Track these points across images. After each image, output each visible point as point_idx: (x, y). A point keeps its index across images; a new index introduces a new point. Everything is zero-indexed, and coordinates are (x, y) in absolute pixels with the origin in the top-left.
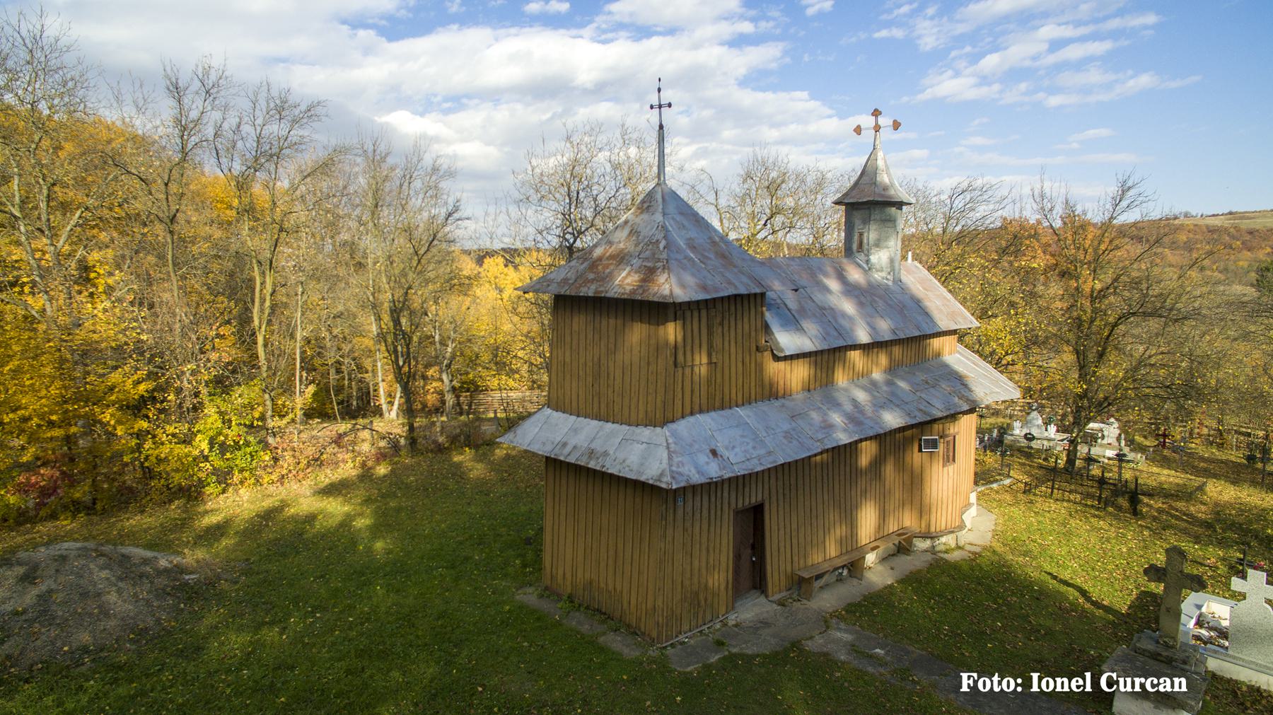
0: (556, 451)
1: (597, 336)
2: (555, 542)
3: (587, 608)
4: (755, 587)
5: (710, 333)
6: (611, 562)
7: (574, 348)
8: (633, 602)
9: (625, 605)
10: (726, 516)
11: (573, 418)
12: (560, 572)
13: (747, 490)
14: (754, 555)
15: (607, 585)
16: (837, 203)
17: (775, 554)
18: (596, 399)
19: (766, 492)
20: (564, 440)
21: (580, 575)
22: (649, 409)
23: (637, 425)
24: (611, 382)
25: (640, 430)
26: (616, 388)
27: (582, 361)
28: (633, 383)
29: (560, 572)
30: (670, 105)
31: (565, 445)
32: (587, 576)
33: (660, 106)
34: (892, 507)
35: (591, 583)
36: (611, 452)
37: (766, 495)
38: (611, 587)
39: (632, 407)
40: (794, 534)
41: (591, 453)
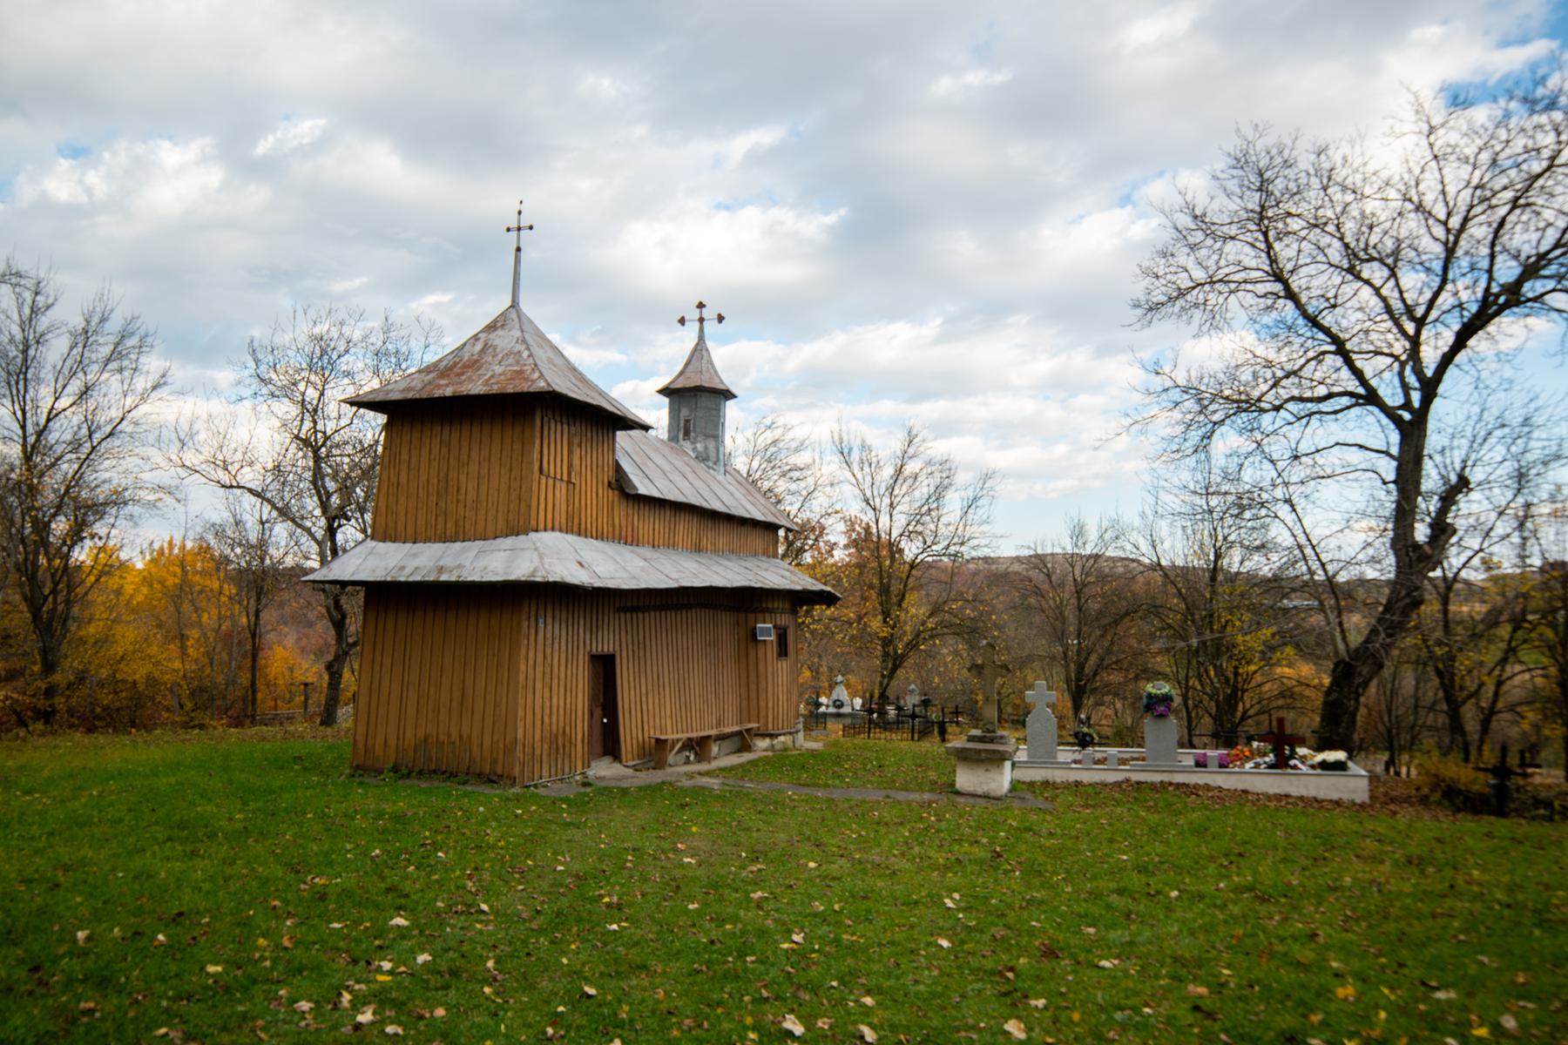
0: (393, 573)
1: (444, 451)
2: (374, 705)
3: (421, 772)
4: (605, 753)
5: (570, 452)
6: (455, 705)
7: (412, 466)
8: (487, 743)
9: (475, 750)
10: (581, 657)
11: (408, 545)
12: (380, 740)
13: (600, 633)
14: (604, 716)
15: (449, 735)
16: (665, 391)
17: (627, 716)
18: (440, 520)
19: (617, 643)
20: (401, 564)
21: (409, 735)
22: (511, 518)
23: (495, 538)
24: (462, 497)
25: (499, 541)
26: (469, 502)
27: (424, 478)
28: (491, 492)
29: (380, 740)
30: (531, 228)
31: (403, 568)
32: (421, 733)
33: (519, 229)
34: (731, 782)
35: (426, 740)
36: (467, 564)
37: (617, 648)
38: (455, 737)
39: (489, 518)
40: (644, 699)
41: (441, 570)
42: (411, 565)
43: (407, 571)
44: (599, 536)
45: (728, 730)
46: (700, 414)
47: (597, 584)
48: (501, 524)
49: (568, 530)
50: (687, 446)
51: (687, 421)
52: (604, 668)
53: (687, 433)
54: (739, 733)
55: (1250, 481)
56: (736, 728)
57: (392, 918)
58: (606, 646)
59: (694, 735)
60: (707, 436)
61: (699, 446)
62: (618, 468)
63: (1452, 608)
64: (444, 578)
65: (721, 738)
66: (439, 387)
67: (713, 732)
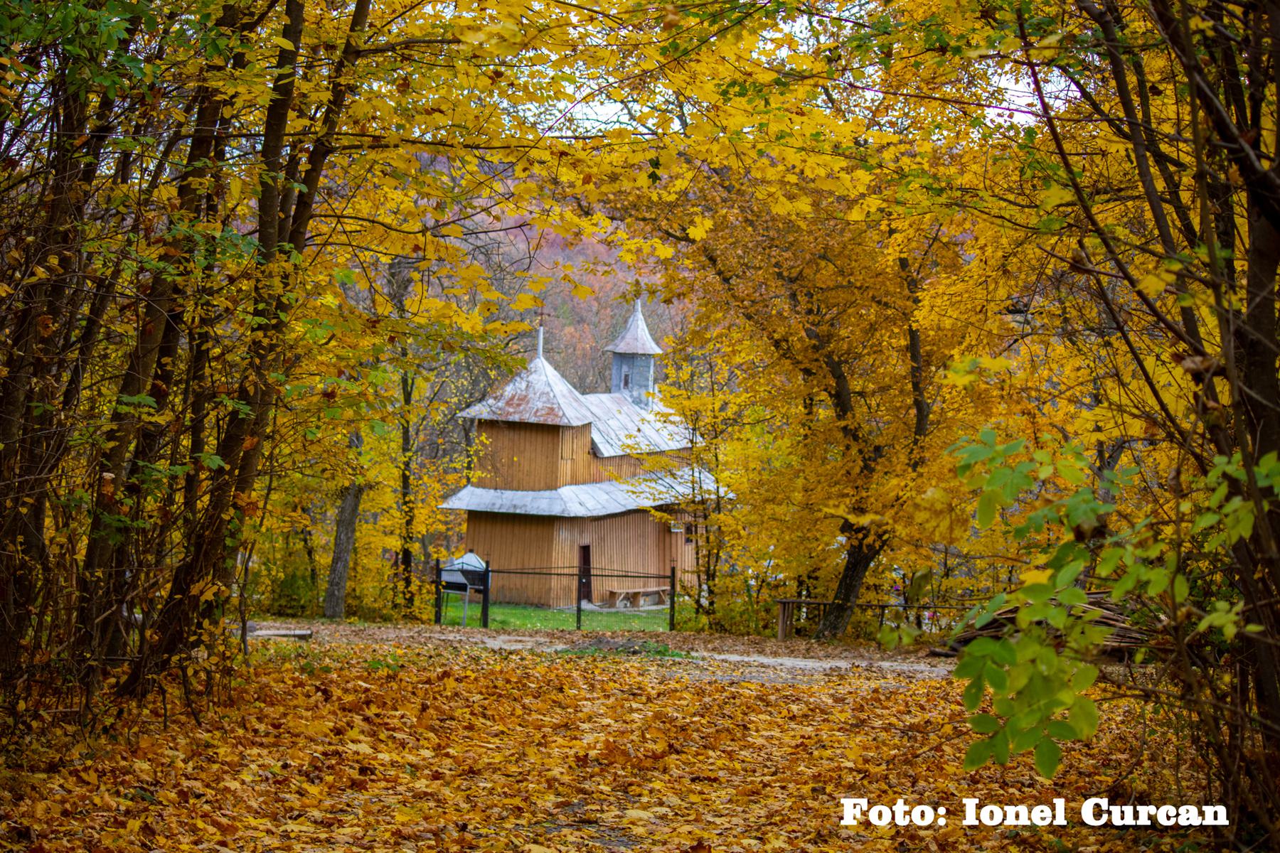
41: (515, 506)
42: (498, 503)
43: (497, 506)
44: (584, 483)
45: (650, 590)
46: (636, 371)
47: (589, 514)
48: (542, 485)
49: (571, 484)
50: (626, 393)
51: (626, 376)
52: (585, 551)
53: (626, 383)
54: (657, 593)
55: (747, 432)
56: (655, 589)
57: (1259, 633)
58: (586, 541)
59: (631, 591)
60: (641, 386)
61: (635, 394)
62: (593, 442)
63: (668, 588)
64: (518, 511)
65: (647, 594)
66: (509, 413)
67: (642, 590)
